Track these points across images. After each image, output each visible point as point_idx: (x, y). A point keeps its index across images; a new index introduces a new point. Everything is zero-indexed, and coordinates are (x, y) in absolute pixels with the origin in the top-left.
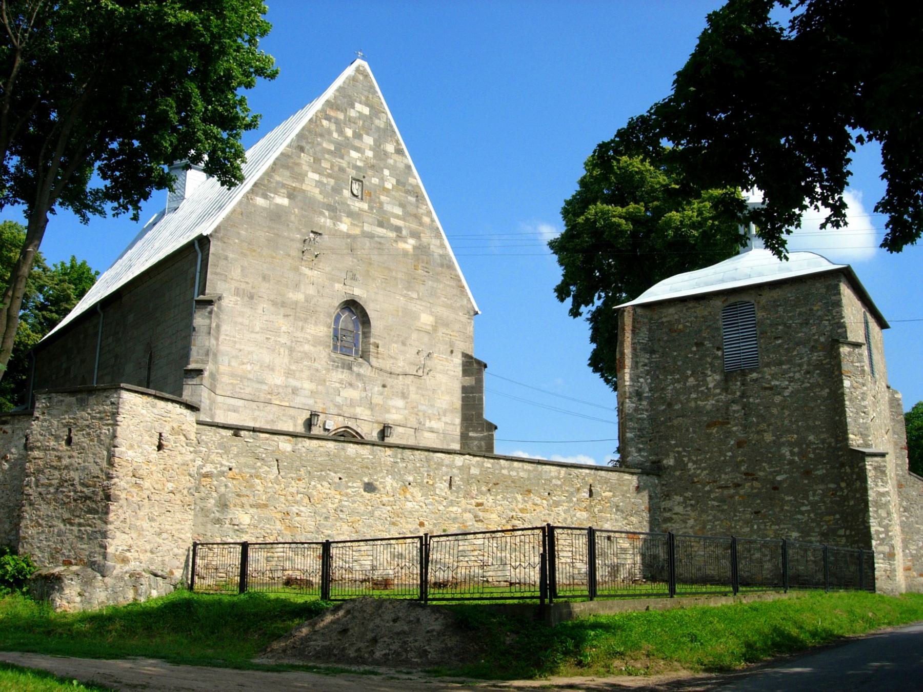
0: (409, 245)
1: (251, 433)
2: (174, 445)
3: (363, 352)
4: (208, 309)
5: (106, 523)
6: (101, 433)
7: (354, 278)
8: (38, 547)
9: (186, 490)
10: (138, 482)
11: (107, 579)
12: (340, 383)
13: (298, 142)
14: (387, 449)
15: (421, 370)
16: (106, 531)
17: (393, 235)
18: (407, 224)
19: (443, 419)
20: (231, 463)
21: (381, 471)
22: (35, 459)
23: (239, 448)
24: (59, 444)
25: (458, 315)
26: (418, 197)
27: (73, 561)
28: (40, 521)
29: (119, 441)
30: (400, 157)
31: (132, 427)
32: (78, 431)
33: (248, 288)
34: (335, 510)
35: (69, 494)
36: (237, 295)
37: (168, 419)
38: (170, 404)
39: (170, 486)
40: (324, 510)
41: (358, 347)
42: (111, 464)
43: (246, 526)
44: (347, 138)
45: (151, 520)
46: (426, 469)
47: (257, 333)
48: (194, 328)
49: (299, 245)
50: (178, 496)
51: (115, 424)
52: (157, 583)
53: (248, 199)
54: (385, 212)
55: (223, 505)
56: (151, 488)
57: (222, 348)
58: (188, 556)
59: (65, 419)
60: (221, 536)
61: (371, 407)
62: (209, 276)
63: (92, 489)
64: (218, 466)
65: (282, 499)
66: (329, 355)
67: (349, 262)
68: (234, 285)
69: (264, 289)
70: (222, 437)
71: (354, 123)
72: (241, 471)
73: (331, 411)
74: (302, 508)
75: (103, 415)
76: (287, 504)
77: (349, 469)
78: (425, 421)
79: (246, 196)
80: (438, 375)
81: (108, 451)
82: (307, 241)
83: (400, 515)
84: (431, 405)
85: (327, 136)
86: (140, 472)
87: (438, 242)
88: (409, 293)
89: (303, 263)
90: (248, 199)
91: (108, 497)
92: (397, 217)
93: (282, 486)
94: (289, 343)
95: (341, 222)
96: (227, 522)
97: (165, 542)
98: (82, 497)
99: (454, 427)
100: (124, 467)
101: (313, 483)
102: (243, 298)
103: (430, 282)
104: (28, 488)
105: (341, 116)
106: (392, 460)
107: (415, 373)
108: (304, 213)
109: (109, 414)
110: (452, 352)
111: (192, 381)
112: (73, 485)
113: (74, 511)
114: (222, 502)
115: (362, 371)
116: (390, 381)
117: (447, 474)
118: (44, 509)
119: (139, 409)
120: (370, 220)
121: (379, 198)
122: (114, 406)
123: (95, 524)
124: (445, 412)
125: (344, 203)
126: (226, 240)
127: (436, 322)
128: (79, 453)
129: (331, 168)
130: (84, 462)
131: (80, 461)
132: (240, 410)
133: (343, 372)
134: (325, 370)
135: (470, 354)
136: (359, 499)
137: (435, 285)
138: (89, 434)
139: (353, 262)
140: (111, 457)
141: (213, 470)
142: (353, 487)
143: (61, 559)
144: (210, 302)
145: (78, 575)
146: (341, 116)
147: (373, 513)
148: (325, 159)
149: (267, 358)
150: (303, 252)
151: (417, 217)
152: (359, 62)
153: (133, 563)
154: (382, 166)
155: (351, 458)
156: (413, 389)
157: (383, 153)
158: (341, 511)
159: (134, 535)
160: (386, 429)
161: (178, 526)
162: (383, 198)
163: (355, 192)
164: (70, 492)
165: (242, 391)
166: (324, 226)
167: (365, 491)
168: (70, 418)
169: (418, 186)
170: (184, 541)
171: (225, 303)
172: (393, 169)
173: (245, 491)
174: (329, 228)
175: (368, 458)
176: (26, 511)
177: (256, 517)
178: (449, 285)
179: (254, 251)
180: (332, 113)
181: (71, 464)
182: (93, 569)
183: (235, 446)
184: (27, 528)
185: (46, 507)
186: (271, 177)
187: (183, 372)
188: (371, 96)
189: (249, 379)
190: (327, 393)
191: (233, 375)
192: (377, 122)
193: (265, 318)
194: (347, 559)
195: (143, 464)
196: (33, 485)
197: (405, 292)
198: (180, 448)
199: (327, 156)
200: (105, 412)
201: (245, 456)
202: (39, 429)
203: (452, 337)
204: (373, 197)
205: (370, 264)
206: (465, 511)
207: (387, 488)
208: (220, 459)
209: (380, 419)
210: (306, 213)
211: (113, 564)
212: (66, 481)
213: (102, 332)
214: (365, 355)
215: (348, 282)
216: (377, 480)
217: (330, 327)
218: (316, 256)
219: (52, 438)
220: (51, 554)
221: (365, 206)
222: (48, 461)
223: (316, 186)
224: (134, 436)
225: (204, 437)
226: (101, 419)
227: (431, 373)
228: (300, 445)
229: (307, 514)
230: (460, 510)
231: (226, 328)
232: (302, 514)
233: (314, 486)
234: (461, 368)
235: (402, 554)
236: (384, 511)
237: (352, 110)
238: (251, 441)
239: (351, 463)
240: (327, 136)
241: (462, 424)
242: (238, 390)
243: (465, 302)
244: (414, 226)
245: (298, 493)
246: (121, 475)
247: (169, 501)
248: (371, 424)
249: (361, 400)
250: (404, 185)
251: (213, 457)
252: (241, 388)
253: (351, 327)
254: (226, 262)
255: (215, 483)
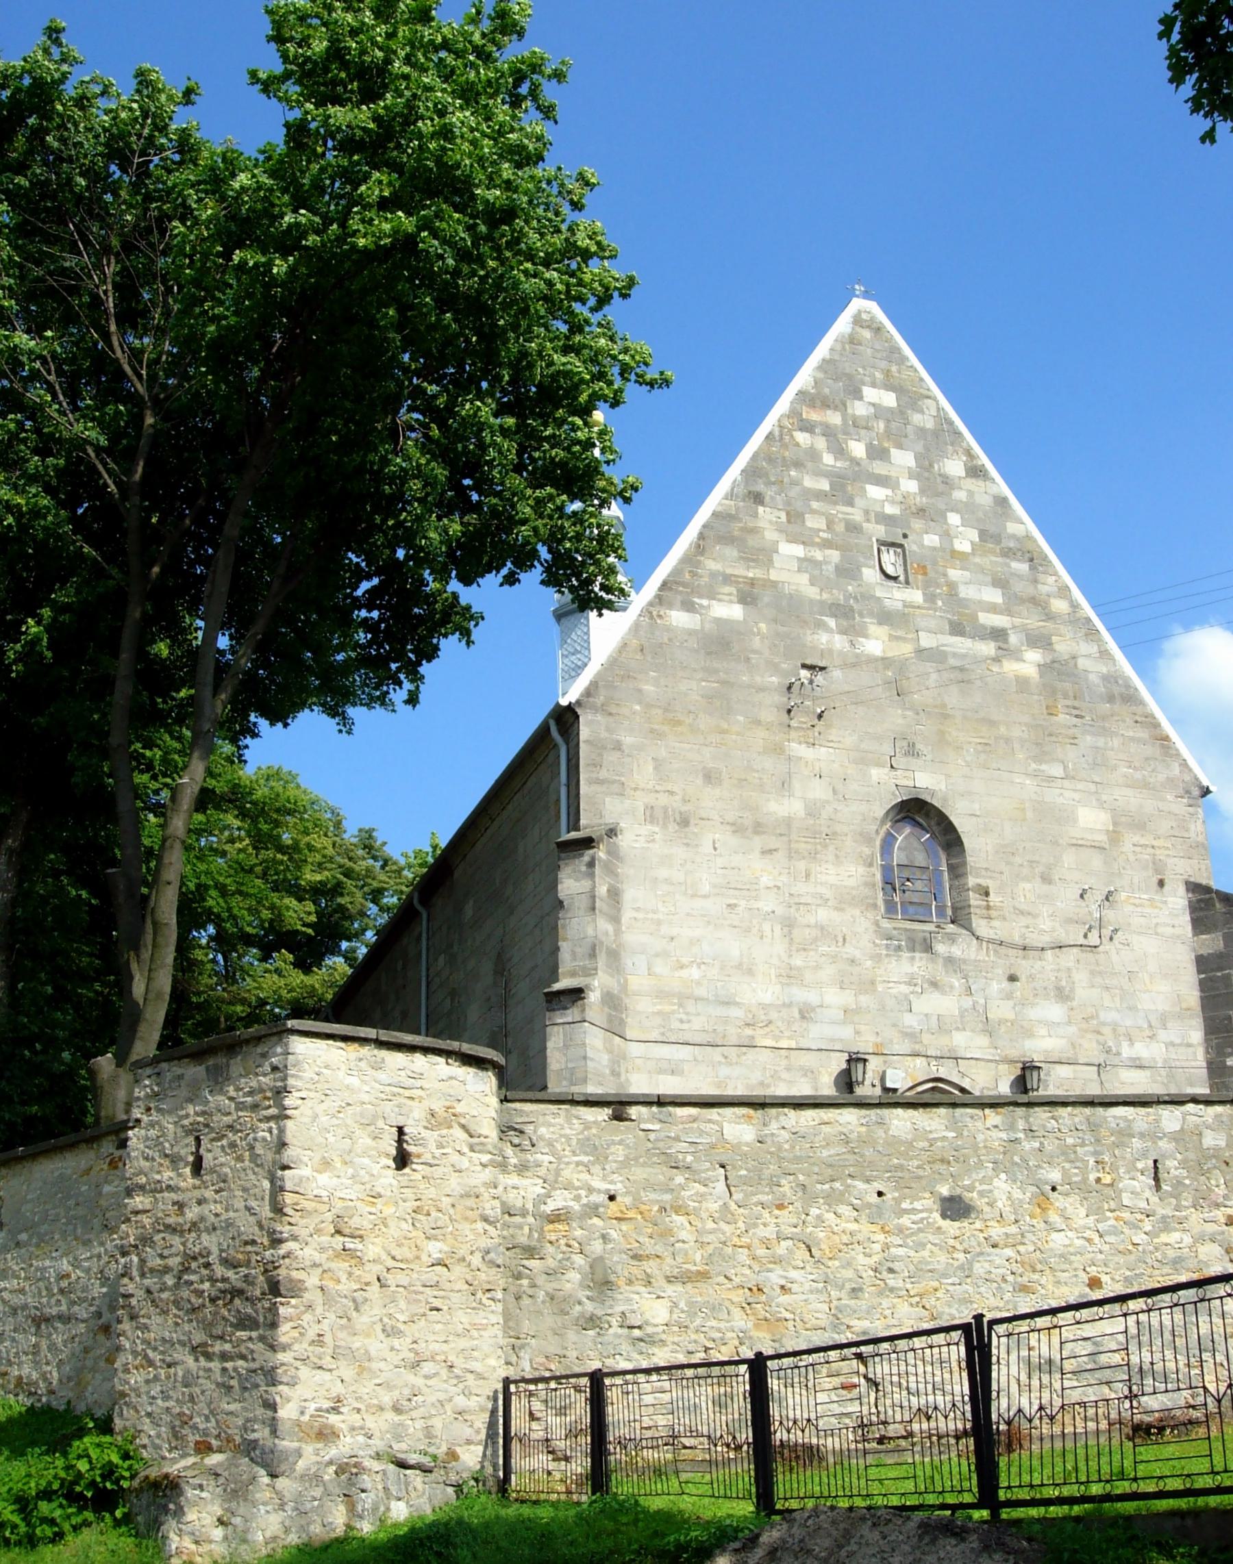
0: (1029, 663)
1: (655, 1109)
2: (438, 1152)
3: (955, 909)
4: (586, 858)
5: (273, 1348)
6: (255, 1139)
7: (911, 751)
8: (149, 1415)
9: (478, 1255)
10: (348, 1246)
11: (281, 1483)
12: (909, 984)
13: (747, 483)
14: (987, 1111)
15: (1095, 933)
16: (274, 1368)
17: (987, 648)
18: (1017, 621)
19: (1163, 1035)
20: (612, 1182)
21: (980, 1164)
22: (137, 1213)
23: (627, 1146)
24: (180, 1175)
25: (1164, 800)
26: (1034, 560)
27: (214, 1443)
28: (150, 1353)
29: (289, 1154)
30: (981, 483)
31: (324, 1119)
32: (213, 1140)
33: (676, 803)
34: (875, 1271)
35: (202, 1287)
36: (652, 822)
37: (419, 1092)
38: (419, 1058)
39: (435, 1249)
40: (849, 1273)
41: (944, 901)
42: (278, 1210)
43: (661, 1328)
44: (855, 462)
45: (390, 1332)
46: (1091, 1149)
47: (705, 897)
48: (561, 903)
49: (780, 699)
50: (458, 1271)
51: (282, 1116)
52: (407, 1484)
53: (652, 617)
54: (963, 603)
55: (602, 1284)
56: (384, 1256)
57: (632, 937)
58: (494, 1412)
59: (187, 1116)
60: (602, 1356)
61: (988, 1028)
62: (584, 789)
63: (243, 1271)
64: (583, 1193)
65: (743, 1255)
66: (877, 924)
67: (896, 718)
68: (640, 802)
69: (711, 801)
70: (587, 1126)
71: (867, 428)
72: (637, 1199)
73: (897, 1049)
74: (794, 1274)
75: (258, 1097)
76: (757, 1268)
77: (900, 1167)
78: (1119, 1045)
79: (647, 611)
80: (1135, 940)
81: (272, 1179)
82: (795, 688)
83: (1039, 1267)
84: (1130, 1008)
85: (809, 465)
86: (355, 1222)
87: (1093, 649)
88: (1044, 767)
89: (793, 734)
90: (652, 617)
91: (274, 1288)
92: (993, 609)
93: (741, 1224)
94: (780, 911)
95: (866, 636)
96: (614, 1323)
97: (430, 1382)
98: (223, 1292)
99: (1191, 1050)
100: (310, 1213)
101: (814, 1211)
102: (665, 826)
103: (1089, 738)
104: (126, 1280)
105: (835, 418)
106: (1004, 1135)
107: (1082, 941)
108: (781, 629)
109: (269, 1094)
110: (1161, 883)
111: (562, 1016)
112: (207, 1265)
113: (211, 1324)
114: (599, 1276)
115: (956, 951)
116: (1024, 966)
117: (1144, 1155)
118: (159, 1326)
119: (341, 1074)
120: (933, 624)
121: (945, 575)
122: (278, 1075)
123: (252, 1351)
124: (1164, 1020)
125: (867, 597)
126: (613, 710)
127: (1115, 824)
128: (217, 1192)
129: (829, 527)
130: (227, 1210)
131: (219, 1208)
132: (686, 1067)
133: (913, 958)
134: (871, 958)
135: (1204, 882)
136: (931, 1237)
137: (1101, 742)
138: (233, 1145)
139: (905, 717)
140: (278, 1189)
141: (572, 1203)
142: (914, 1211)
143: (192, 1438)
144: (588, 843)
145: (217, 1475)
146: (835, 418)
147: (971, 1269)
148: (813, 512)
149: (734, 948)
150: (789, 711)
151: (1038, 603)
152: (857, 304)
153: (348, 1439)
154: (943, 507)
155: (902, 1142)
156: (1081, 977)
157: (939, 480)
158: (891, 1270)
159: (348, 1372)
160: (1028, 1074)
161: (463, 1343)
162: (954, 574)
163: (890, 570)
164: (202, 1282)
165: (685, 1026)
166: (830, 651)
167: (944, 1216)
168: (197, 1114)
169: (1029, 537)
170: (480, 1377)
171: (625, 841)
172: (968, 510)
173: (650, 1246)
174: (841, 653)
175: (944, 1138)
176: (123, 1333)
177: (682, 1305)
178: (1132, 739)
179: (679, 723)
180: (814, 416)
181: (202, 1219)
182: (252, 1460)
183: (620, 1143)
184: (127, 1371)
185: (159, 1319)
186: (698, 564)
187: (542, 998)
188: (894, 368)
189: (697, 999)
190: (882, 1008)
191: (661, 995)
192: (916, 418)
193: (720, 862)
194: (913, 1386)
195: (359, 1204)
196: (135, 1273)
197: (1034, 766)
198: (455, 1158)
199: (815, 505)
200: (262, 1091)
201: (644, 1165)
202: (142, 1146)
203: (1158, 852)
204: (931, 574)
205: (946, 717)
206: (1200, 1239)
207: (1000, 1204)
208: (585, 1176)
209: (1014, 1053)
210: (785, 629)
211: (296, 1444)
212: (195, 1258)
213: (428, 950)
214: (960, 917)
215: (900, 761)
216: (971, 1189)
217: (871, 865)
218: (820, 716)
219: (167, 1162)
220: (173, 1428)
221: (916, 596)
222: (160, 1215)
223: (799, 570)
224: (331, 1139)
225: (543, 1130)
226: (255, 1107)
227: (1119, 937)
228: (774, 1126)
229: (807, 1286)
230: (1187, 1240)
231: (632, 895)
232: (795, 1287)
233: (819, 1217)
234: (1188, 918)
235: (1050, 1361)
236: (998, 1261)
237: (857, 403)
238: (657, 1127)
239: (905, 1155)
240: (809, 465)
241: (1207, 1040)
242: (676, 1025)
243: (1176, 770)
244: (1033, 622)
245: (780, 1238)
246: (303, 1233)
247: (436, 1285)
248: (993, 1065)
249: (962, 1017)
250: (997, 539)
251: (567, 1173)
252: (682, 1021)
253: (920, 859)
254: (617, 754)
255: (578, 1233)
